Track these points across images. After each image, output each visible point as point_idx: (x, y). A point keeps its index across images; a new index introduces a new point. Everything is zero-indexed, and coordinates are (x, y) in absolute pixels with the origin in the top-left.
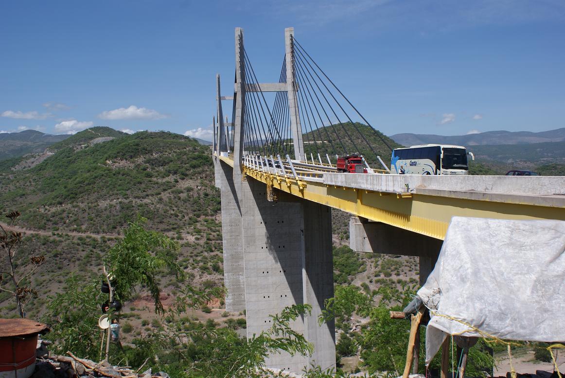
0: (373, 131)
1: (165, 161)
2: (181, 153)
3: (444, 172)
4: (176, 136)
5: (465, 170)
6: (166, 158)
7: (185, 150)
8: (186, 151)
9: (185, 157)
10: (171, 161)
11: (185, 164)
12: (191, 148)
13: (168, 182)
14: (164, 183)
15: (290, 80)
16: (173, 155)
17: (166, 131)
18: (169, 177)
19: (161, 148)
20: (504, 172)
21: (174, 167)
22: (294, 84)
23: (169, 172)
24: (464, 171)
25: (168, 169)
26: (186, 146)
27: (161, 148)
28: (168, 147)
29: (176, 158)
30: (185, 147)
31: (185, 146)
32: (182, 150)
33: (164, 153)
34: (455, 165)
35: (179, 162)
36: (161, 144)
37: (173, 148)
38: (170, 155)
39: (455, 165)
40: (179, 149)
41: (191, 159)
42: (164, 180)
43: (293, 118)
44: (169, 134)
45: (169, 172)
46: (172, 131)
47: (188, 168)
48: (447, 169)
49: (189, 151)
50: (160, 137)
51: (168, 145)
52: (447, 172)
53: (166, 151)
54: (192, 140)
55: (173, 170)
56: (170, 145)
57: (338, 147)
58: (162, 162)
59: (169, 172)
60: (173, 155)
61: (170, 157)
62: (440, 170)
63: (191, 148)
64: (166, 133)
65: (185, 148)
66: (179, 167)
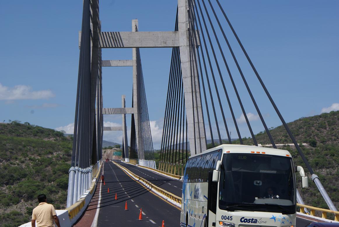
0: (278, 128)
1: (12, 176)
2: (42, 161)
3: (224, 217)
4: (41, 131)
5: (284, 213)
6: (15, 170)
7: (50, 156)
8: (51, 159)
9: (49, 168)
10: (25, 176)
11: (49, 181)
12: (61, 153)
13: (16, 214)
14: (8, 216)
15: (184, 25)
16: (28, 166)
17: (23, 122)
18: (19, 205)
19: (8, 153)
20: (13, 225)
21: (29, 186)
22: (192, 32)
23: (20, 195)
24: (279, 216)
25: (18, 190)
26: (53, 149)
27: (8, 153)
28: (20, 150)
29: (33, 171)
30: (51, 150)
31: (53, 147)
32: (46, 157)
33: (12, 161)
34: (258, 201)
35: (38, 179)
36: (8, 146)
37: (28, 153)
38: (24, 166)
39: (258, 201)
40: (40, 155)
41: (61, 173)
42: (9, 210)
43: (188, 97)
44: (28, 128)
45: (18, 195)
46: (34, 122)
47: (54, 189)
48: (233, 210)
49: (58, 158)
50: (11, 132)
51: (20, 147)
52: (230, 218)
53: (16, 159)
54: (67, 137)
55: (26, 192)
56: (24, 146)
57: (327, 155)
58: (8, 177)
59: (20, 195)
60: (28, 166)
61: (22, 168)
62: (215, 212)
63: (61, 153)
64: (23, 125)
65: (51, 153)
66: (38, 186)
